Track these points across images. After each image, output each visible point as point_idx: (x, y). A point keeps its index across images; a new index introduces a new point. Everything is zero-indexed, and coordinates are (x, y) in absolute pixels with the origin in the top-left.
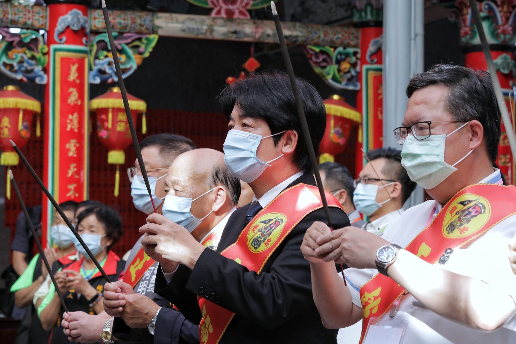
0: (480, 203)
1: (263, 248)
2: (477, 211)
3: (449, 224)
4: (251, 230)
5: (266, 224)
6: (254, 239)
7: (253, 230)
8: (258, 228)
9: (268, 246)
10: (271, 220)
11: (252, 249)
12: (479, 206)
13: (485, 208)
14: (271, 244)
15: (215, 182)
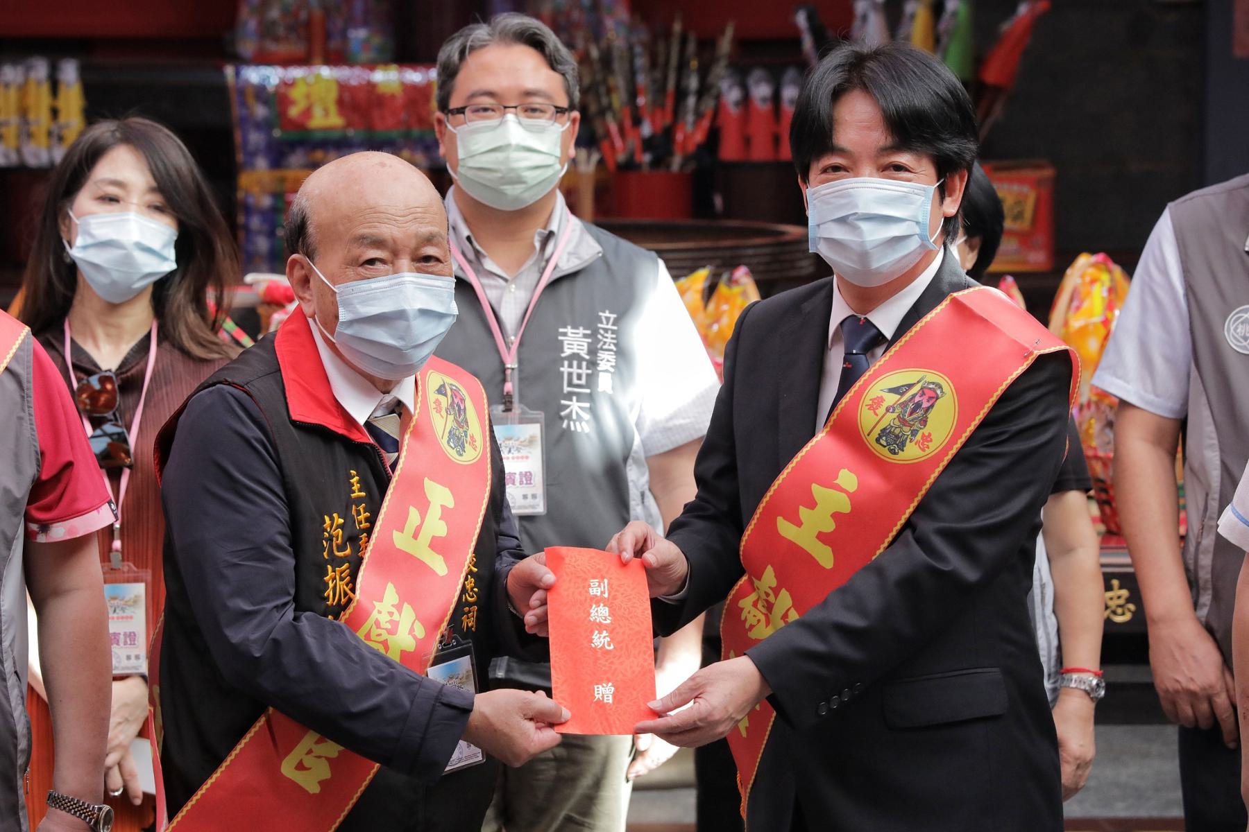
1: (912, 452)
2: (930, 398)
3: (446, 434)
4: (865, 409)
5: (902, 394)
6: (883, 430)
7: (871, 407)
8: (885, 405)
9: (928, 451)
10: (910, 386)
11: (884, 453)
13: (940, 387)
14: (935, 446)
15: (534, 110)
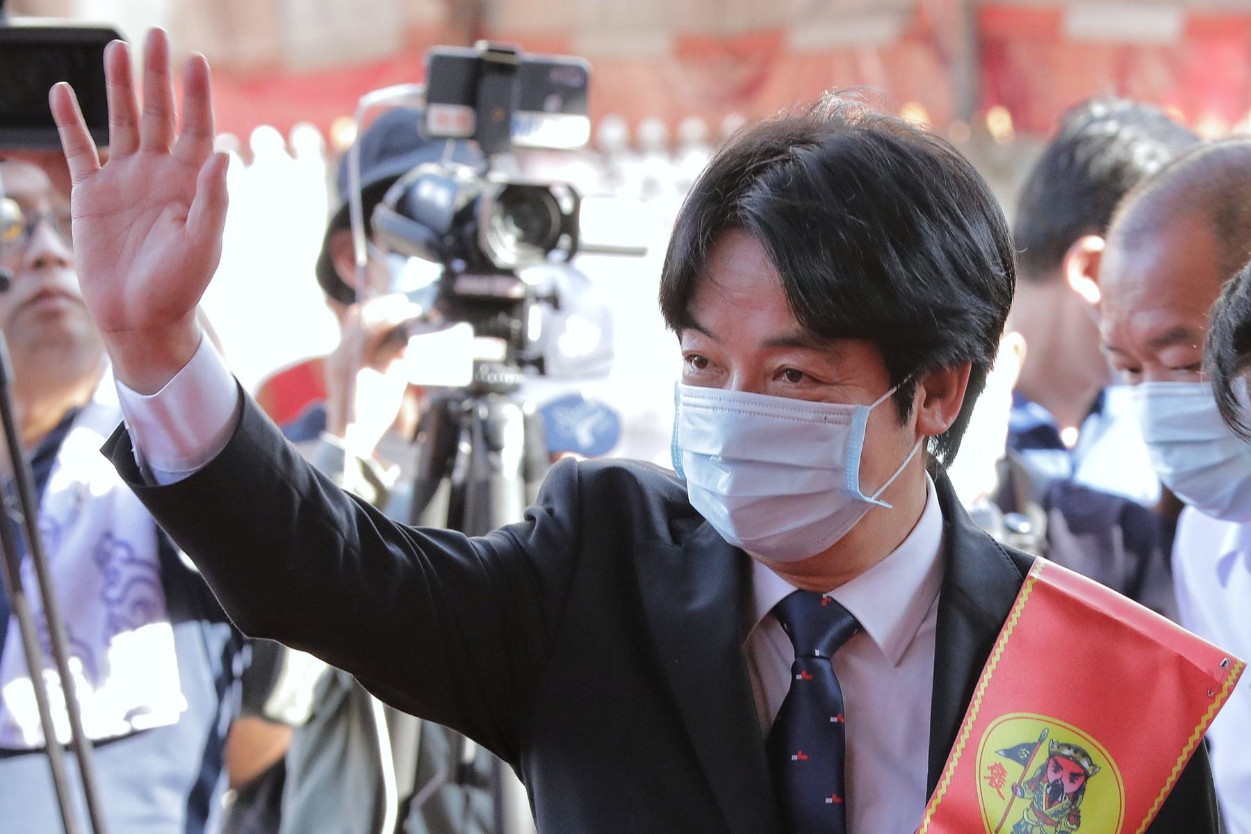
0: (1060, 745)
12: (1067, 757)
13: (1085, 755)
